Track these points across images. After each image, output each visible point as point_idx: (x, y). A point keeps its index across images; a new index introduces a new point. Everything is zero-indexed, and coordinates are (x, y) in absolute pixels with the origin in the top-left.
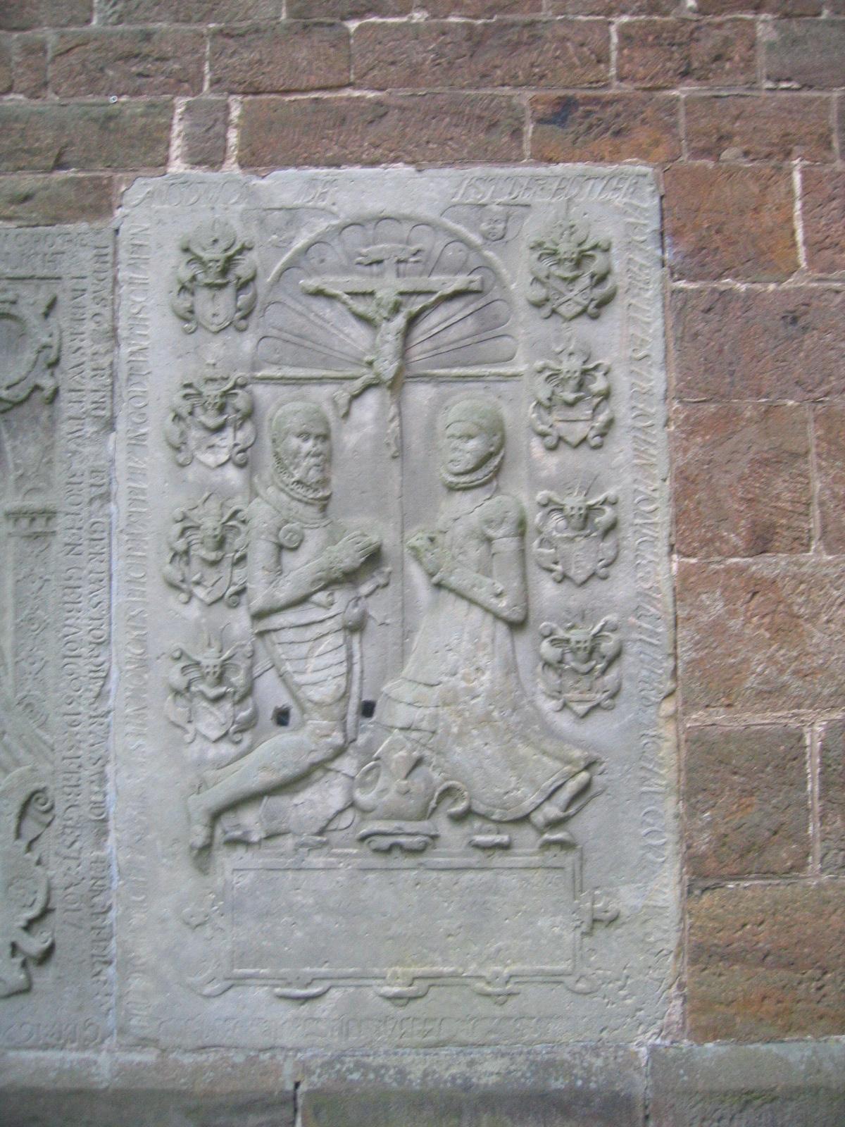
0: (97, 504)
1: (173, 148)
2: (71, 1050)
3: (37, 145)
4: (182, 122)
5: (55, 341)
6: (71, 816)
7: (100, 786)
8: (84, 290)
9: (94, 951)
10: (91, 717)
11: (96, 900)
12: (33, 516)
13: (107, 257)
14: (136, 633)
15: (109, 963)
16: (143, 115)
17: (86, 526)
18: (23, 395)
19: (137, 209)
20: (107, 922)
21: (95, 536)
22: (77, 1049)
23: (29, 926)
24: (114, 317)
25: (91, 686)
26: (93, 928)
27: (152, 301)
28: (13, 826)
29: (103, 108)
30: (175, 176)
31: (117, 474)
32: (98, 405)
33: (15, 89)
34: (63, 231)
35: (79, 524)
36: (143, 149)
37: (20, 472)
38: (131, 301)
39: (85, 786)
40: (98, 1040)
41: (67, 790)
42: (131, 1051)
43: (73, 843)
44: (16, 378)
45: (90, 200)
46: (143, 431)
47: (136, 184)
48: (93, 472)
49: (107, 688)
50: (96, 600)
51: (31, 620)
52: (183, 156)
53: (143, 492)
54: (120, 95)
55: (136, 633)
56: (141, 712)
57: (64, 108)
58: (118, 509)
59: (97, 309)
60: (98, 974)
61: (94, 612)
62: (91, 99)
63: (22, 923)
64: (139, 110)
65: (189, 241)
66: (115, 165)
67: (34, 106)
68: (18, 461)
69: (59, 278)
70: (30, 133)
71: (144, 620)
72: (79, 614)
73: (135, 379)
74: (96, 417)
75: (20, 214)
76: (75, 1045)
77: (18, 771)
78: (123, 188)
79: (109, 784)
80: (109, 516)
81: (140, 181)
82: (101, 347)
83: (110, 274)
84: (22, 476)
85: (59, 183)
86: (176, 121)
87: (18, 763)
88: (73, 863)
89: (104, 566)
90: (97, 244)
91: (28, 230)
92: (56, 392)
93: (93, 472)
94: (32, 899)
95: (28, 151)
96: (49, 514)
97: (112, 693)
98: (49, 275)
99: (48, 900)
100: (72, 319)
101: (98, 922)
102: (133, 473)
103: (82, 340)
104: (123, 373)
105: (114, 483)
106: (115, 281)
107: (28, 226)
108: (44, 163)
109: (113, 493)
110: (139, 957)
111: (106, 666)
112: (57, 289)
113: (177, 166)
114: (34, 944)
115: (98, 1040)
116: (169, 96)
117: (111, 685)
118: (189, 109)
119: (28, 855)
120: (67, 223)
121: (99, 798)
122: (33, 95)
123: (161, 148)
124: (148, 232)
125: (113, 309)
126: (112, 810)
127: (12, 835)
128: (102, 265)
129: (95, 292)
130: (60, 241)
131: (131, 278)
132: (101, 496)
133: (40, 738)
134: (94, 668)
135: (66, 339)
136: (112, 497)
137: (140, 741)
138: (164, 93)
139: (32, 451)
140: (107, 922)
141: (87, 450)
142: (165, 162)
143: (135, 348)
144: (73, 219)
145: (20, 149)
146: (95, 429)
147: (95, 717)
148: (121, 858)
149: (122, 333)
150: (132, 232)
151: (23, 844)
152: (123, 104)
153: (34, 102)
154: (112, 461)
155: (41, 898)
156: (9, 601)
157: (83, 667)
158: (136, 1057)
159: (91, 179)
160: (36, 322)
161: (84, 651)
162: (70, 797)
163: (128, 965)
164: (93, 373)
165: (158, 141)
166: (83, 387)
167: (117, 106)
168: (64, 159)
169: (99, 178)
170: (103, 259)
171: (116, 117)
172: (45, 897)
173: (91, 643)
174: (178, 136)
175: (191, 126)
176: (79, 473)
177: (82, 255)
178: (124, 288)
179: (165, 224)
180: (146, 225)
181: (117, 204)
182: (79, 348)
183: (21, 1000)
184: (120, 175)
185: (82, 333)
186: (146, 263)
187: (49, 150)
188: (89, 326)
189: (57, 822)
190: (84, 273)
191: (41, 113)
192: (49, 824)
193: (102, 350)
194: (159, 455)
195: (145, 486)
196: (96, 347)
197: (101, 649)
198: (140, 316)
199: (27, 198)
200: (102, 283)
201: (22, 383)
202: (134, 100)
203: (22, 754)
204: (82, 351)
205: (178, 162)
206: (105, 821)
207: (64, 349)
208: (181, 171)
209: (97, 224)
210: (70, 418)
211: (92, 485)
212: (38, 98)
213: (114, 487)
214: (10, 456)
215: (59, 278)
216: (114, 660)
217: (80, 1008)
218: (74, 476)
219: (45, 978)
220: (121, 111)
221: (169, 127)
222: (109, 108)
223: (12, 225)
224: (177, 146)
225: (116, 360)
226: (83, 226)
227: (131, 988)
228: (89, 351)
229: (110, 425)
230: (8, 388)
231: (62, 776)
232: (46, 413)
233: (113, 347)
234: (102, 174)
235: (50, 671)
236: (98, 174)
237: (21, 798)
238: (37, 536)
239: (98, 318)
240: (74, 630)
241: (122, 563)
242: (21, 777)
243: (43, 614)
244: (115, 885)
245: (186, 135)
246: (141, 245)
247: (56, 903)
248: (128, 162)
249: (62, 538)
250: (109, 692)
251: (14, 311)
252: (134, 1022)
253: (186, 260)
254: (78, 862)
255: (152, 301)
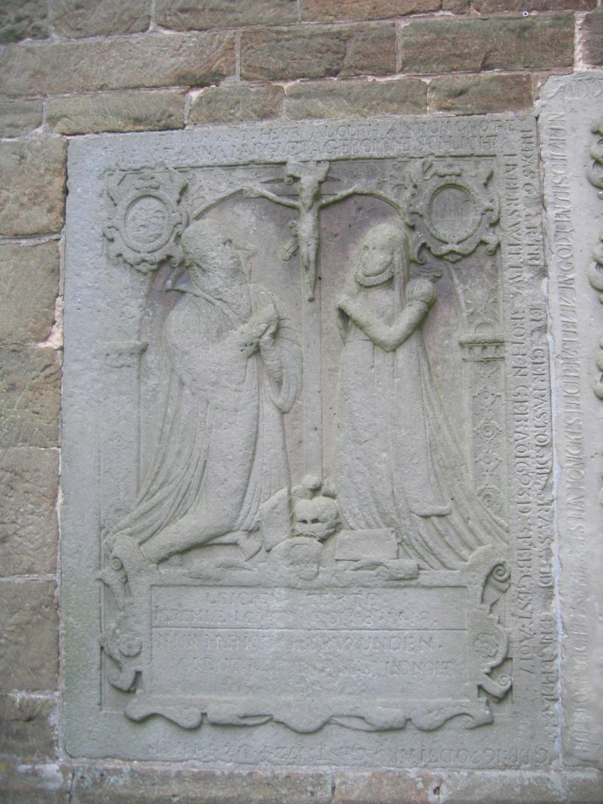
0: (536, 334)
1: (576, 52)
2: (525, 769)
3: (466, 50)
4: (581, 32)
5: (496, 206)
6: (524, 584)
7: (547, 560)
8: (515, 165)
9: (544, 692)
10: (539, 505)
11: (545, 650)
12: (484, 345)
13: (531, 139)
14: (573, 437)
15: (556, 700)
16: (551, 26)
17: (529, 353)
18: (471, 249)
19: (552, 101)
20: (555, 668)
21: (537, 360)
22: (530, 769)
23: (493, 671)
24: (542, 187)
25: (538, 481)
26: (544, 673)
27: (571, 174)
28: (479, 594)
29: (517, 21)
30: (581, 74)
31: (551, 311)
32: (534, 256)
33: (443, 8)
34: (494, 119)
35: (524, 351)
36: (554, 53)
37: (471, 310)
38: (553, 173)
39: (535, 559)
40: (547, 762)
41: (521, 563)
42: (574, 771)
43: (526, 606)
44: (465, 235)
45: (513, 94)
46: (570, 276)
47: (549, 81)
48: (532, 309)
49: (550, 482)
50: (540, 411)
51: (486, 429)
52: (586, 59)
53: (574, 325)
54: (530, 11)
55: (573, 437)
56: (579, 500)
57: (486, 22)
58: (554, 340)
59: (527, 180)
60: (547, 709)
61: (538, 422)
62: (507, 14)
63: (487, 670)
64: (547, 22)
65: (598, 126)
66: (532, 65)
67: (461, 20)
68: (469, 302)
69: (495, 156)
70: (460, 41)
71: (580, 427)
72: (527, 423)
73: (561, 235)
74: (531, 265)
75: (458, 106)
76: (528, 766)
77: (480, 549)
78: (539, 84)
79: (553, 558)
80: (547, 344)
81: (554, 78)
82: (531, 211)
83: (535, 152)
84: (472, 313)
85: (486, 81)
86: (576, 31)
87: (480, 543)
88: (526, 622)
89: (546, 384)
90: (523, 128)
91: (465, 117)
92: (499, 245)
93: (532, 309)
94: (494, 651)
95: (458, 56)
96: (498, 343)
97: (555, 486)
98: (486, 153)
99: (507, 653)
100: (507, 188)
101: (548, 668)
102: (565, 310)
103: (516, 205)
104: (551, 232)
105: (549, 318)
106: (540, 158)
107: (464, 115)
108: (473, 65)
109: (549, 326)
110: (582, 695)
111: (549, 464)
112: (493, 165)
113: (581, 67)
114: (497, 686)
115: (547, 762)
116: (570, 11)
117: (554, 479)
118: (588, 20)
119: (491, 616)
120: (496, 112)
121: (546, 569)
122: (460, 12)
123: (568, 52)
124: (563, 119)
125: (540, 180)
126: (556, 579)
127: (478, 600)
128: (527, 145)
129: (524, 166)
130: (493, 127)
131: (552, 155)
132: (539, 329)
133: (497, 522)
134: (540, 466)
135: (504, 204)
136: (548, 330)
137: (580, 524)
138: (567, 8)
139: (480, 293)
140: (555, 668)
141: (526, 292)
142: (571, 64)
143: (559, 211)
144: (503, 109)
145: (453, 54)
146: (531, 275)
147: (542, 505)
148: (565, 617)
149: (548, 199)
150: (549, 119)
151: (487, 607)
152: (534, 17)
153: (460, 17)
154: (547, 300)
155: (502, 650)
156: (467, 413)
157: (532, 465)
158: (580, 775)
159: (512, 77)
160: (477, 190)
161: (531, 452)
162: (523, 569)
163: (571, 702)
164: (527, 231)
165: (566, 46)
166: (520, 242)
167: (529, 20)
168: (489, 61)
169: (519, 76)
170: (528, 140)
171: (530, 27)
172: (506, 650)
173: (537, 446)
174: (580, 42)
175: (590, 34)
176: (521, 310)
177: (511, 137)
178: (547, 163)
179: (576, 112)
180: (562, 113)
181: (535, 97)
182: (515, 211)
183: (486, 730)
184: (536, 74)
185: (517, 199)
186: (564, 144)
187: (477, 55)
188: (522, 193)
189: (513, 588)
190: (513, 152)
191: (468, 26)
192: (505, 592)
193: (533, 213)
194: (585, 295)
195: (575, 320)
196: (529, 211)
197: (545, 450)
198: (562, 185)
199: (462, 93)
200: (529, 160)
201: (469, 239)
202: (542, 14)
203: (483, 535)
204: (517, 213)
205: (581, 63)
206: (552, 587)
207: (503, 211)
208: (585, 70)
209: (521, 113)
210: (511, 267)
211: (532, 320)
212: (462, 14)
213: (550, 321)
214: (462, 298)
215: (495, 156)
216: (555, 459)
217: (532, 737)
218: (516, 313)
219: (503, 713)
220: (533, 23)
221: (572, 35)
222: (523, 21)
223: (451, 114)
224: (579, 51)
225: (544, 220)
226: (510, 114)
227: (576, 720)
228: (523, 214)
229: (543, 272)
230: (458, 243)
231: (516, 552)
232: (488, 265)
233: (541, 210)
234: (521, 73)
235: (504, 468)
236: (518, 73)
237: (487, 571)
238: (487, 361)
239: (529, 187)
240: (523, 436)
241: (559, 381)
242: (486, 553)
243: (496, 423)
244: (560, 638)
245: (587, 42)
246: (558, 129)
247: (514, 655)
248: (543, 63)
249: (511, 362)
250: (552, 485)
251: (459, 182)
252: (577, 747)
253: (597, 140)
254: (531, 620)
255: (571, 174)
